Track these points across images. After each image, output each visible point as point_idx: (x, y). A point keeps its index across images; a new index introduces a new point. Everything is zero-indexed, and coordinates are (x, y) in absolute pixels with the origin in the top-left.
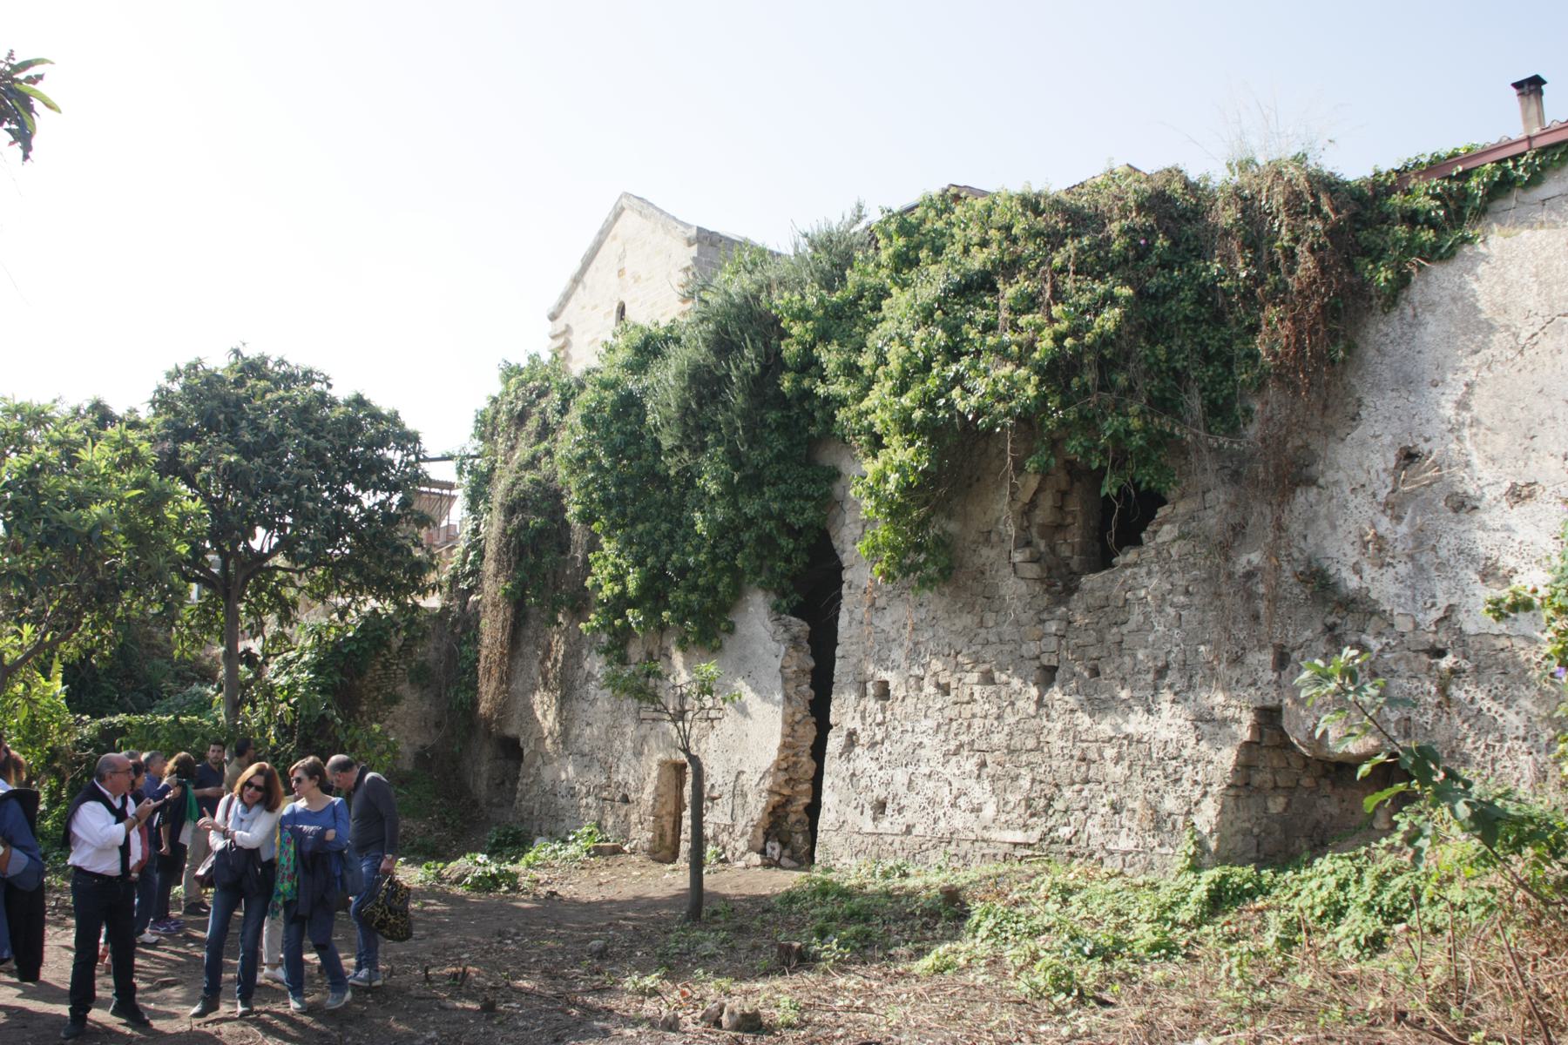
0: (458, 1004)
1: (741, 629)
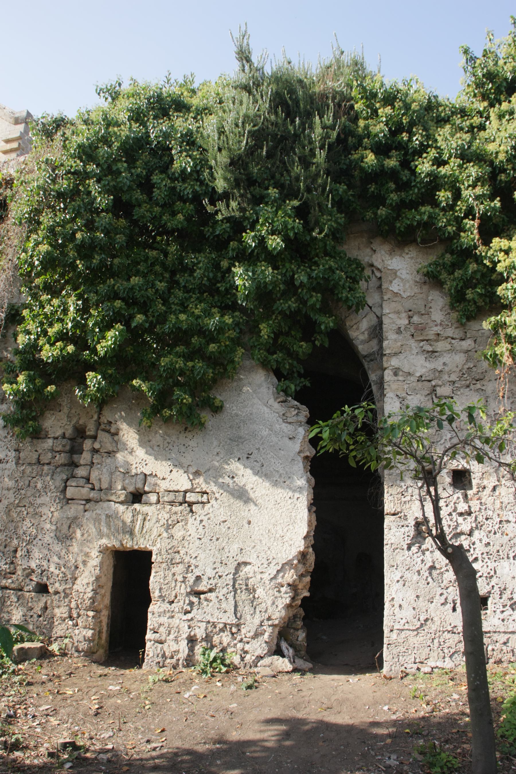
0: (218, 746)
1: (232, 408)
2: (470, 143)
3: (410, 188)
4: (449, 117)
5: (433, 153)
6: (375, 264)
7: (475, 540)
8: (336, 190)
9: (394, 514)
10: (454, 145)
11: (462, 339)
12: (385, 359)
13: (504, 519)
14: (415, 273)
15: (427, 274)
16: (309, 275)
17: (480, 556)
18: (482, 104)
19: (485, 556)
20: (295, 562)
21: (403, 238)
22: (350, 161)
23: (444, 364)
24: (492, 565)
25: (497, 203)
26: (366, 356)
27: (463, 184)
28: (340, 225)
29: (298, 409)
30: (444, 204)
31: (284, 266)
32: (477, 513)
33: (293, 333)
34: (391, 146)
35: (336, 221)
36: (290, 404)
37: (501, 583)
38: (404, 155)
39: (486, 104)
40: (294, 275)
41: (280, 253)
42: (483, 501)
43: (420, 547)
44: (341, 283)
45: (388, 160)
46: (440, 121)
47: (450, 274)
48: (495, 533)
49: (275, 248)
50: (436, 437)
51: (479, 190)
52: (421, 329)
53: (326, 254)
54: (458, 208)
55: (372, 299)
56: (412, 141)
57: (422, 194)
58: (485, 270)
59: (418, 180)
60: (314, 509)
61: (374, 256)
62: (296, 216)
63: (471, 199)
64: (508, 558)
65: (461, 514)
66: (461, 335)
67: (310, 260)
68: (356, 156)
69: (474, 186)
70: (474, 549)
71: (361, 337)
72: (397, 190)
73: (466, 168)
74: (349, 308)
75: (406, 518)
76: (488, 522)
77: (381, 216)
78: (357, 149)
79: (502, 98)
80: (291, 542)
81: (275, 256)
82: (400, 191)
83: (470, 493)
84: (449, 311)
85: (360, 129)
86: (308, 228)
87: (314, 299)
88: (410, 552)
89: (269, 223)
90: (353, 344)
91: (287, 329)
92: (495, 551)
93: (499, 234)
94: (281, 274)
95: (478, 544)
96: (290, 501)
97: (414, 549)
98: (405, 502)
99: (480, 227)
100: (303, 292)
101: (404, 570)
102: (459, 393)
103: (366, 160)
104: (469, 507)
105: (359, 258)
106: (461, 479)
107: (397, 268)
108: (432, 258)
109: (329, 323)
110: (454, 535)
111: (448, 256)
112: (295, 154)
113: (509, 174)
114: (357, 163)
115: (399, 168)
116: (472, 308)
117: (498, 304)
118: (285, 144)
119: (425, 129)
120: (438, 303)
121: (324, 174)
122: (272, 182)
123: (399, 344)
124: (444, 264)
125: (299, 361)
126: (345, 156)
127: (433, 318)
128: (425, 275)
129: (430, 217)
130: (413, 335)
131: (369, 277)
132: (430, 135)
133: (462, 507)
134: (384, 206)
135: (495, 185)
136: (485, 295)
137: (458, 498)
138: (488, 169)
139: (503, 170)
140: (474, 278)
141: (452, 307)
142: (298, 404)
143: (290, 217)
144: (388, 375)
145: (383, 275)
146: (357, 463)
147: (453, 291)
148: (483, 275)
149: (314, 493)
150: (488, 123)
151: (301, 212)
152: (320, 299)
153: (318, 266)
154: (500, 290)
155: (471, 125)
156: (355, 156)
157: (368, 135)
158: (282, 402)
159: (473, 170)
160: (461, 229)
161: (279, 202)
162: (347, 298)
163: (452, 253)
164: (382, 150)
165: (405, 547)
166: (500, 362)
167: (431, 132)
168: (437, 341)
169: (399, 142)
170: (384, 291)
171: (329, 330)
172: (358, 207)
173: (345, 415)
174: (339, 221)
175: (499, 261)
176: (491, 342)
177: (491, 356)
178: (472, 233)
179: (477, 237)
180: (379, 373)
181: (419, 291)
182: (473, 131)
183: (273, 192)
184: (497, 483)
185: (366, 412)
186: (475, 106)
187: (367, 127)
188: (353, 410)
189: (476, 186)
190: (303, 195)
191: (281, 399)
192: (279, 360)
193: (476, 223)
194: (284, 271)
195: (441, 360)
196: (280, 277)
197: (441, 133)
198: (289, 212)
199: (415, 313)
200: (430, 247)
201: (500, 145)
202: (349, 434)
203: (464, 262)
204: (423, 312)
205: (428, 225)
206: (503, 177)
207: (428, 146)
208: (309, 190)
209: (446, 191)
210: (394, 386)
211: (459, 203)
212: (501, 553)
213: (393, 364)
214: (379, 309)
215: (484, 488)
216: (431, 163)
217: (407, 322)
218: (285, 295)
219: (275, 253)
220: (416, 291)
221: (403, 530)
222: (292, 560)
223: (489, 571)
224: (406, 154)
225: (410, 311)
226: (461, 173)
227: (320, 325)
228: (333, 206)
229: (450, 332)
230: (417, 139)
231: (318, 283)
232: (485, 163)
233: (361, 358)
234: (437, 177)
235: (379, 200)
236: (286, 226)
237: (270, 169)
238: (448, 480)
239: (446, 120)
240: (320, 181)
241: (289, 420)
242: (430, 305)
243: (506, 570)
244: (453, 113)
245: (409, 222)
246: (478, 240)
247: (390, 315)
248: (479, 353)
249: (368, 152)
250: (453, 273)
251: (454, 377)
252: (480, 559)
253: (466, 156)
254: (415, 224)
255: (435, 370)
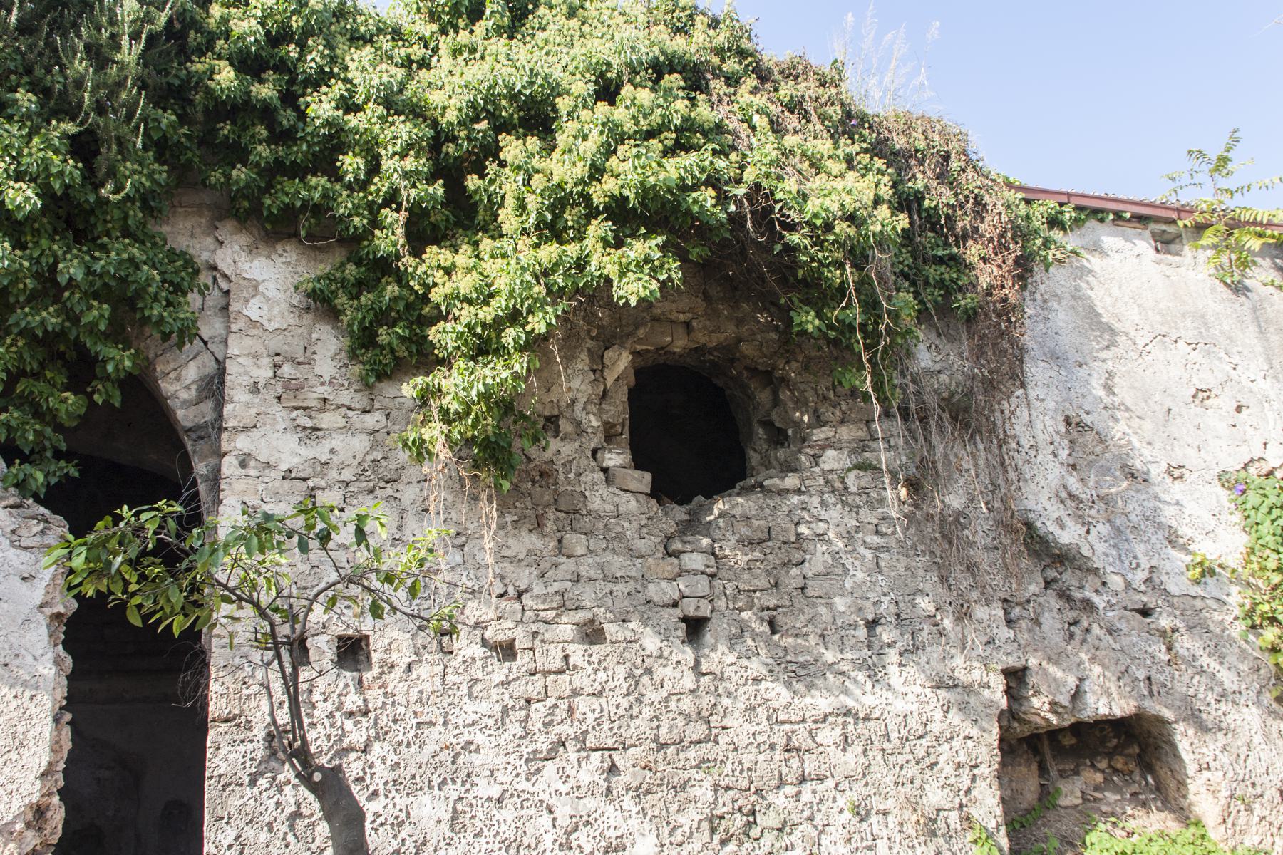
2: (402, 87)
3: (295, 140)
4: (372, 36)
5: (338, 88)
6: (220, 266)
7: (374, 759)
8: (156, 120)
9: (226, 721)
10: (376, 82)
11: (365, 411)
12: (225, 436)
13: (426, 719)
14: (292, 289)
15: (312, 294)
16: (88, 268)
17: (381, 787)
18: (428, 27)
19: (390, 786)
20: (19, 826)
21: (276, 228)
22: (189, 72)
23: (332, 451)
24: (402, 802)
25: (438, 189)
26: (190, 430)
27: (386, 149)
28: (159, 184)
29: (46, 521)
30: (350, 177)
31: (36, 243)
32: (379, 711)
33: (49, 374)
34: (268, 62)
35: (150, 176)
36: (29, 512)
37: (418, 832)
38: (287, 82)
39: (435, 27)
40: (56, 263)
41: (30, 218)
42: (389, 690)
43: (274, 779)
44: (151, 290)
45: (257, 85)
46: (358, 39)
47: (352, 299)
48: (409, 745)
49: (19, 207)
50: (310, 578)
51: (410, 163)
52: (295, 388)
53: (126, 233)
54: (373, 188)
55: (210, 327)
56: (305, 61)
57: (314, 154)
58: (412, 298)
59: (309, 129)
60: (68, 717)
61: (219, 252)
62: (68, 153)
63: (396, 175)
64: (430, 787)
65: (351, 714)
66: (365, 403)
67: (94, 240)
68: (199, 67)
69: (403, 156)
70: (372, 776)
71: (184, 395)
72: (269, 141)
73: (393, 124)
74: (166, 337)
75: (249, 726)
76: (397, 727)
77: (237, 182)
78: (204, 54)
79: (461, 23)
80: (10, 787)
81: (20, 223)
82: (277, 144)
83: (368, 676)
84: (347, 361)
85: (212, 21)
86: (92, 179)
87: (95, 312)
88: (255, 791)
89: (13, 158)
90: (168, 407)
91: (35, 366)
92: (408, 777)
93: (437, 241)
94: (30, 259)
95: (379, 766)
96: (14, 703)
97: (263, 783)
98: (248, 697)
99: (408, 225)
100: (73, 299)
101: (242, 824)
102: (355, 502)
103: (217, 77)
104: (365, 700)
105: (191, 251)
106: (352, 651)
107: (260, 279)
108: (324, 268)
109: (122, 360)
110: (337, 752)
111: (351, 268)
112: (80, 37)
113: (462, 146)
114: (200, 80)
115: (277, 103)
116: (388, 359)
117: (431, 358)
118: (62, 15)
119: (329, 45)
120: (328, 345)
121: (134, 84)
122: (26, 79)
123: (253, 411)
124: (343, 279)
125: (59, 428)
126: (180, 64)
127: (318, 370)
128: (309, 296)
129: (325, 196)
130: (279, 398)
131: (207, 287)
132: (336, 57)
133: (353, 701)
134: (245, 165)
135: (437, 159)
136: (410, 340)
137: (346, 686)
138: (429, 133)
139: (454, 139)
140: (392, 309)
141: (353, 355)
142: (47, 512)
143: (56, 152)
144: (229, 466)
145: (233, 287)
146: (145, 618)
147: (355, 328)
148: (408, 306)
149: (69, 686)
150: (435, 58)
151: (83, 147)
152: (107, 314)
153: (108, 252)
154: (433, 334)
155: (408, 56)
156: (199, 66)
157: (227, 34)
158: (11, 507)
159: (404, 129)
160: (376, 223)
161: (37, 120)
162: (161, 319)
163: (358, 264)
164: (249, 65)
165: (246, 780)
166: (429, 452)
167: (338, 52)
168: (322, 410)
169: (281, 58)
170: (232, 315)
171: (122, 375)
172: (196, 160)
173: (122, 524)
174: (157, 176)
175: (435, 285)
176: (415, 420)
177: (414, 442)
178: (393, 233)
179: (402, 241)
180: (212, 461)
181: (296, 321)
182: (410, 68)
183: (25, 99)
184: (414, 658)
185: (164, 518)
186: (416, 28)
187: (225, 20)
188: (137, 515)
189: (407, 155)
190: (87, 115)
191: (11, 501)
192: (13, 423)
193: (403, 216)
194: (36, 254)
195: (327, 445)
196: (26, 264)
197: (355, 57)
198: (56, 142)
199: (286, 360)
200: (320, 249)
201: (450, 97)
202: (129, 562)
203: (379, 281)
204: (301, 359)
205: (320, 210)
206: (450, 148)
207: (332, 75)
208: (100, 109)
209: (355, 155)
210: (239, 486)
211: (376, 179)
212: (418, 780)
213: (239, 446)
214: (222, 347)
215: (393, 667)
216: (333, 104)
217: (271, 374)
218: (34, 299)
219: (20, 216)
220: (292, 321)
221: (242, 748)
222: (13, 823)
223: (397, 812)
224: (292, 82)
225: (278, 355)
226: (382, 129)
227: (105, 361)
228: (145, 148)
229: (345, 397)
230: (313, 60)
231: (106, 285)
232: (425, 121)
233: (181, 433)
234: (342, 129)
235: (238, 153)
236: (47, 169)
237: (23, 55)
238: (330, 654)
239: (367, 40)
240: (124, 96)
241: (24, 543)
242: (315, 348)
243: (427, 811)
244: (380, 30)
245: (287, 200)
246: (403, 246)
247: (240, 360)
248: (394, 436)
249: (223, 63)
250: (357, 297)
251: (347, 475)
252: (382, 792)
253: (392, 103)
254: (298, 204)
255: (315, 461)
